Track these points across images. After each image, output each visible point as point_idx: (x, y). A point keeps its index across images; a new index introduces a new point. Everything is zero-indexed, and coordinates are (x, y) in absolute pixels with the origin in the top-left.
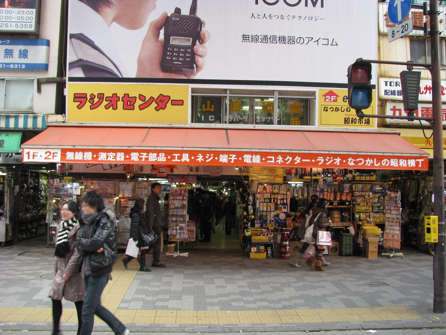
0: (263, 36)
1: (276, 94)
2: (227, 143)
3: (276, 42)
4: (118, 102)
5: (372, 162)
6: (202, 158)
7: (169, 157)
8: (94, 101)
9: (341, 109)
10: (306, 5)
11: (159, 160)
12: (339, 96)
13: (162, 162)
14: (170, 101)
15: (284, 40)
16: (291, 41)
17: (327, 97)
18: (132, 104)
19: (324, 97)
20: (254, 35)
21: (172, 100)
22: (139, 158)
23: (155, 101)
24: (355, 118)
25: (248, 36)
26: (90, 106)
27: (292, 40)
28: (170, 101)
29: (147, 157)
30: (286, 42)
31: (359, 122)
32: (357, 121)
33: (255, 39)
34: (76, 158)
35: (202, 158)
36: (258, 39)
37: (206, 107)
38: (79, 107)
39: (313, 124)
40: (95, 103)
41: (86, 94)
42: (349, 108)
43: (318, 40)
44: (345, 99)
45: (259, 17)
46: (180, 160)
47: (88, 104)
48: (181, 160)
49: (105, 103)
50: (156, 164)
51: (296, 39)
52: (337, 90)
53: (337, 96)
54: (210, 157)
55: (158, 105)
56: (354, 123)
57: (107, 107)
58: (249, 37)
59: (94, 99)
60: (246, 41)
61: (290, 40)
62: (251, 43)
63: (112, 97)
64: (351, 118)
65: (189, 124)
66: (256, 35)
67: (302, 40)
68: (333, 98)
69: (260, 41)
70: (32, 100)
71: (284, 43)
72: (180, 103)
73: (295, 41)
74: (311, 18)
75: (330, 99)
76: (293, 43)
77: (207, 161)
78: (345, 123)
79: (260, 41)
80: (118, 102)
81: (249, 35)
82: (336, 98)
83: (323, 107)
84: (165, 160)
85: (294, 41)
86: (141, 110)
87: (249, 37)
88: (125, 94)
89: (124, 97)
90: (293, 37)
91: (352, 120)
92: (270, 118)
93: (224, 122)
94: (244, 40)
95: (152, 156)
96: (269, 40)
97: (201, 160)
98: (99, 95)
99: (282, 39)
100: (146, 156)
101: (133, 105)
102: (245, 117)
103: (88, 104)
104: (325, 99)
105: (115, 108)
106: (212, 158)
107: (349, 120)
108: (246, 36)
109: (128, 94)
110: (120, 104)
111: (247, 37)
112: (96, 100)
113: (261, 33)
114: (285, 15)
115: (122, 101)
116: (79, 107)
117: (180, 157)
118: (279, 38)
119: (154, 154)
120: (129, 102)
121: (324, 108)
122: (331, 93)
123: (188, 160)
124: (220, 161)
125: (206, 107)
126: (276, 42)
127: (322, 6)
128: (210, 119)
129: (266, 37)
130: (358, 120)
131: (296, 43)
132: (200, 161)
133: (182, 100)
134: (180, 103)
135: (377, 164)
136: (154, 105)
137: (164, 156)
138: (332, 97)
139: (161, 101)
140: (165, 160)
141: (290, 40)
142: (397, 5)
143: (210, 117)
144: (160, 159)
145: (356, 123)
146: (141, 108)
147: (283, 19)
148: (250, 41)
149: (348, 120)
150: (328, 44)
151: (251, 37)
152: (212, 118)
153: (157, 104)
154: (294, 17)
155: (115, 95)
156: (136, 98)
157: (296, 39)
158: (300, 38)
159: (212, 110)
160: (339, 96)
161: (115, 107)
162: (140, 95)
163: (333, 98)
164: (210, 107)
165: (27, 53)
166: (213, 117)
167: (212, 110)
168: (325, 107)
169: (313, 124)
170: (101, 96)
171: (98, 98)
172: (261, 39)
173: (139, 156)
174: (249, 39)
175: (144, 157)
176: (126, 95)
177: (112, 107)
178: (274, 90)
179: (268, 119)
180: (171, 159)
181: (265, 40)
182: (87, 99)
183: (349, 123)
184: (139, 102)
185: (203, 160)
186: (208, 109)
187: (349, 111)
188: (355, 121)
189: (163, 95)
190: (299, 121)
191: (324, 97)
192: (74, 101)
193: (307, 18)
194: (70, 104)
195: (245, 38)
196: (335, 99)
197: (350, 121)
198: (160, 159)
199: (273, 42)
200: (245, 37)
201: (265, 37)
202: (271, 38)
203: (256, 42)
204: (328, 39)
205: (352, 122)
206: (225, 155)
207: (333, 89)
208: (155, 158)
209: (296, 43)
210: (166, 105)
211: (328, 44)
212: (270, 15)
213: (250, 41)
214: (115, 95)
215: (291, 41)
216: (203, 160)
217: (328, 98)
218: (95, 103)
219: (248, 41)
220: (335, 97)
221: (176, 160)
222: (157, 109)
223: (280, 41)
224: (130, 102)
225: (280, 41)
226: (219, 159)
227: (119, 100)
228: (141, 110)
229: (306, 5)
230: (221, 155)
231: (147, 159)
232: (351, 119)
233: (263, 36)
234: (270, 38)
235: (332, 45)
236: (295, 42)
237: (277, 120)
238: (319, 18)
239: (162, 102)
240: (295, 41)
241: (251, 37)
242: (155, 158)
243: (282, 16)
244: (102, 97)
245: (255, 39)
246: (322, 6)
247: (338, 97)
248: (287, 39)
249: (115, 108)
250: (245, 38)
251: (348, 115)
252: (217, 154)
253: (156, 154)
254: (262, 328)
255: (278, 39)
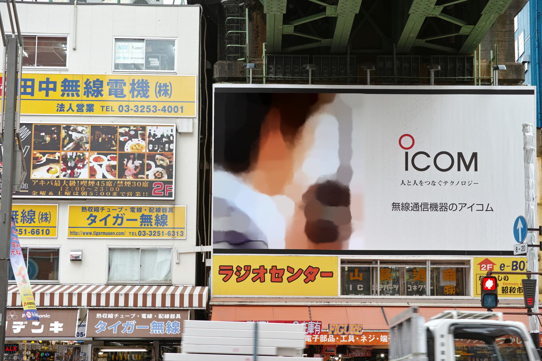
0: (414, 204)
1: (428, 263)
2: (386, 324)
3: (427, 209)
4: (265, 274)
5: (514, 340)
6: (366, 338)
7: (337, 338)
8: (240, 273)
9: (498, 278)
10: (459, 169)
11: (329, 341)
12: (495, 264)
13: (331, 342)
14: (319, 273)
15: (435, 208)
16: (443, 208)
17: (482, 266)
18: (280, 276)
19: (479, 265)
20: (404, 203)
21: (321, 272)
22: (312, 339)
23: (304, 273)
24: (514, 287)
25: (398, 204)
26: (237, 279)
27: (444, 207)
28: (319, 273)
29: (319, 338)
30: (438, 209)
31: (519, 291)
32: (516, 290)
33: (405, 207)
34: (116, 277)
35: (366, 338)
36: (408, 207)
37: (354, 276)
38: (225, 280)
39: (469, 295)
40: (241, 275)
41: (232, 266)
42: (507, 277)
43: (471, 206)
44: (503, 267)
45: (409, 184)
46: (347, 341)
47: (234, 277)
48: (348, 341)
49: (252, 275)
50: (325, 344)
51: (448, 206)
52: (491, 257)
53: (494, 264)
54: (372, 338)
55: (307, 277)
56: (513, 293)
57: (254, 280)
58: (399, 206)
59: (240, 271)
60: (396, 210)
61: (442, 207)
62: (401, 211)
63: (260, 269)
64: (509, 287)
65: (339, 295)
66: (407, 203)
67: (454, 206)
68: (489, 266)
69: (410, 209)
70: (170, 271)
71: (436, 210)
72: (330, 274)
73: (448, 208)
74: (463, 183)
75: (486, 268)
76: (446, 210)
77: (370, 341)
78: (503, 293)
79: (410, 209)
80: (265, 274)
81: (399, 204)
82: (493, 266)
83: (479, 276)
84: (334, 341)
85: (446, 208)
86: (289, 282)
87: (399, 206)
88: (272, 266)
89: (272, 269)
90: (445, 204)
91: (510, 290)
92: (422, 286)
93: (374, 292)
94: (394, 209)
95: (323, 338)
96: (420, 208)
97: (365, 341)
98: (246, 268)
99: (434, 207)
100: (318, 337)
101: (281, 277)
102: (396, 286)
103: (234, 277)
104: (481, 268)
105: (263, 281)
106: (374, 338)
107: (508, 289)
108: (396, 204)
109: (276, 266)
110: (268, 276)
111: (397, 206)
112: (243, 272)
113: (411, 200)
114: (437, 181)
115: (270, 273)
116: (225, 280)
117: (347, 338)
118: (431, 205)
119: (325, 336)
120: (277, 275)
121: (480, 277)
122: (487, 262)
123: (353, 341)
124: (381, 341)
125: (354, 276)
126: (427, 209)
127: (476, 170)
128: (359, 289)
129: (416, 204)
130: (518, 289)
131: (448, 210)
132: (364, 341)
133: (332, 272)
134: (330, 274)
135: (519, 342)
136: (303, 277)
137: (333, 337)
138: (488, 265)
139: (310, 273)
140: (334, 341)
141: (442, 207)
142: (519, 229)
143: (358, 286)
144: (329, 340)
145: (515, 292)
146: (290, 280)
147: (434, 185)
148: (400, 209)
149: (506, 289)
150: (483, 210)
151: (402, 206)
152: (360, 287)
153: (306, 276)
154: (446, 183)
155: (262, 267)
156: (284, 270)
157: (448, 206)
158: (453, 204)
159: (361, 279)
160: (495, 264)
161: (262, 280)
162: (288, 267)
163: (489, 266)
164: (359, 276)
165: (167, 219)
166: (362, 286)
167: (361, 279)
168: (481, 276)
169: (469, 295)
170: (248, 268)
171: (244, 270)
172: (412, 207)
173: (312, 337)
174: (399, 208)
175: (316, 338)
176: (274, 267)
177: (259, 279)
178: (426, 260)
179: (421, 287)
180: (339, 340)
181: (416, 208)
182: (233, 271)
183: (507, 293)
184: (287, 274)
185: (366, 340)
186: (356, 278)
187: (506, 279)
188: (514, 290)
189: (312, 267)
190: (453, 289)
191: (479, 265)
192: (219, 274)
193: (460, 183)
194: (214, 277)
195: (395, 206)
196: (491, 267)
197: (509, 291)
198: (329, 340)
199: (424, 209)
200: (395, 206)
201: (416, 205)
202: (422, 205)
203: (406, 210)
204: (483, 205)
205: (510, 292)
206: (385, 336)
207: (490, 257)
208: (325, 339)
209: (448, 210)
210: (315, 277)
211: (483, 210)
212: (421, 181)
213: (400, 209)
214: (262, 267)
215: (443, 208)
216: (366, 340)
217: (484, 266)
218: (241, 275)
219: (398, 209)
220: (492, 265)
221: (344, 341)
222: (306, 281)
223: (432, 208)
224: (279, 274)
225: (432, 208)
226: (380, 339)
227: (267, 273)
228: (289, 282)
229: (459, 169)
230: (382, 336)
231: (318, 340)
232: (509, 288)
233: (414, 204)
234: (421, 206)
235: (487, 210)
236: (447, 209)
237: (430, 288)
238: (473, 182)
239: (311, 274)
240: (448, 208)
241: (402, 206)
242: (325, 339)
243: (433, 181)
244: (249, 269)
245: (405, 207)
246: (476, 170)
247: (494, 266)
248: (439, 206)
249: (263, 281)
250: (395, 206)
251: (506, 284)
252: (378, 334)
253: (326, 336)
254: (484, 23)
255: (429, 206)
